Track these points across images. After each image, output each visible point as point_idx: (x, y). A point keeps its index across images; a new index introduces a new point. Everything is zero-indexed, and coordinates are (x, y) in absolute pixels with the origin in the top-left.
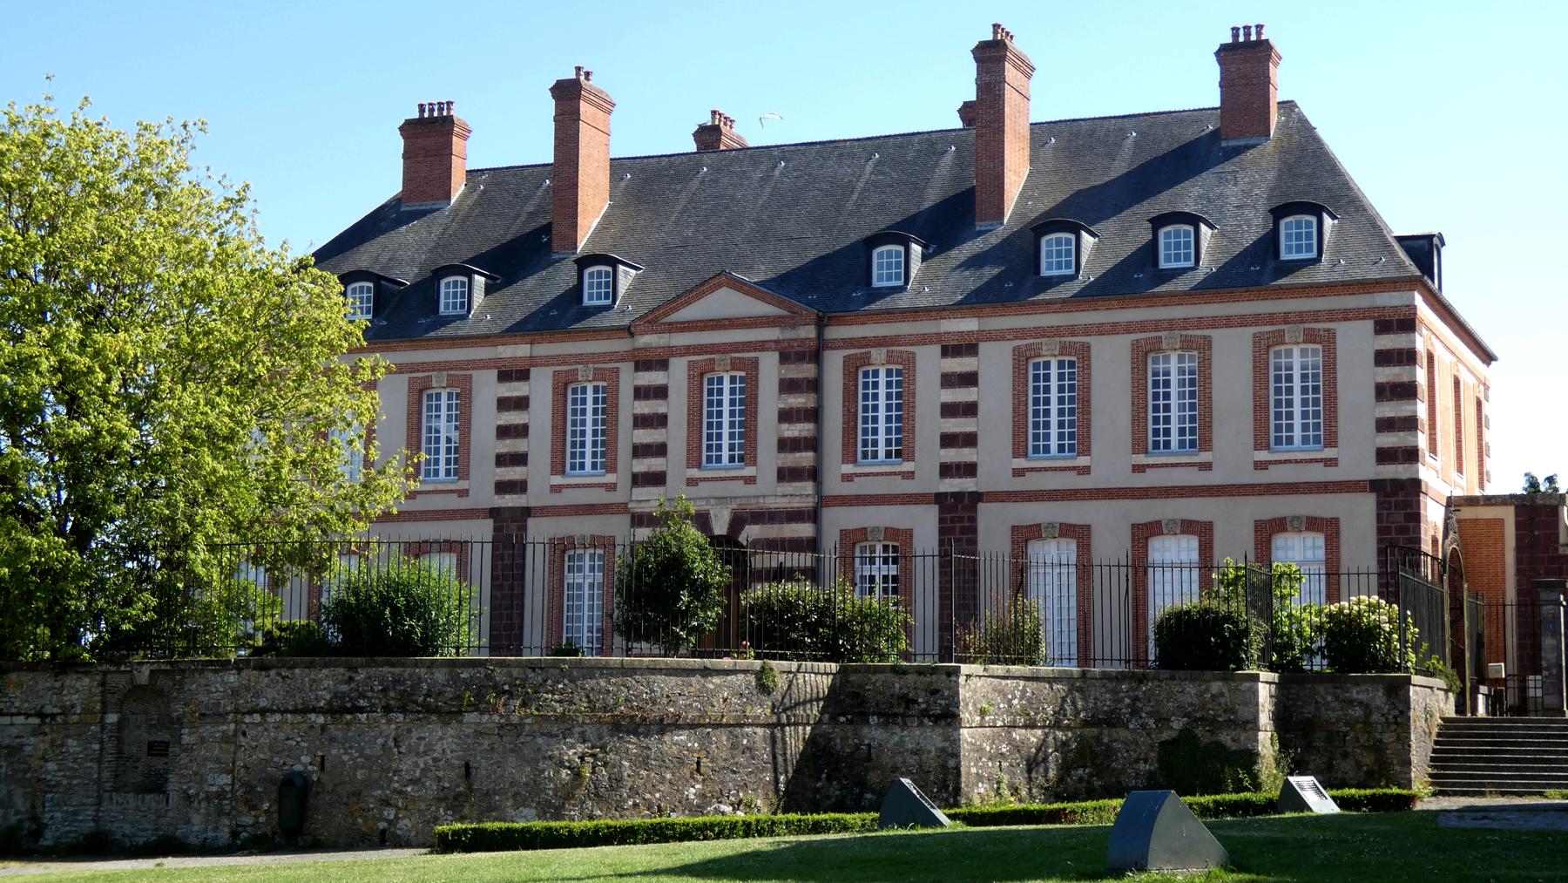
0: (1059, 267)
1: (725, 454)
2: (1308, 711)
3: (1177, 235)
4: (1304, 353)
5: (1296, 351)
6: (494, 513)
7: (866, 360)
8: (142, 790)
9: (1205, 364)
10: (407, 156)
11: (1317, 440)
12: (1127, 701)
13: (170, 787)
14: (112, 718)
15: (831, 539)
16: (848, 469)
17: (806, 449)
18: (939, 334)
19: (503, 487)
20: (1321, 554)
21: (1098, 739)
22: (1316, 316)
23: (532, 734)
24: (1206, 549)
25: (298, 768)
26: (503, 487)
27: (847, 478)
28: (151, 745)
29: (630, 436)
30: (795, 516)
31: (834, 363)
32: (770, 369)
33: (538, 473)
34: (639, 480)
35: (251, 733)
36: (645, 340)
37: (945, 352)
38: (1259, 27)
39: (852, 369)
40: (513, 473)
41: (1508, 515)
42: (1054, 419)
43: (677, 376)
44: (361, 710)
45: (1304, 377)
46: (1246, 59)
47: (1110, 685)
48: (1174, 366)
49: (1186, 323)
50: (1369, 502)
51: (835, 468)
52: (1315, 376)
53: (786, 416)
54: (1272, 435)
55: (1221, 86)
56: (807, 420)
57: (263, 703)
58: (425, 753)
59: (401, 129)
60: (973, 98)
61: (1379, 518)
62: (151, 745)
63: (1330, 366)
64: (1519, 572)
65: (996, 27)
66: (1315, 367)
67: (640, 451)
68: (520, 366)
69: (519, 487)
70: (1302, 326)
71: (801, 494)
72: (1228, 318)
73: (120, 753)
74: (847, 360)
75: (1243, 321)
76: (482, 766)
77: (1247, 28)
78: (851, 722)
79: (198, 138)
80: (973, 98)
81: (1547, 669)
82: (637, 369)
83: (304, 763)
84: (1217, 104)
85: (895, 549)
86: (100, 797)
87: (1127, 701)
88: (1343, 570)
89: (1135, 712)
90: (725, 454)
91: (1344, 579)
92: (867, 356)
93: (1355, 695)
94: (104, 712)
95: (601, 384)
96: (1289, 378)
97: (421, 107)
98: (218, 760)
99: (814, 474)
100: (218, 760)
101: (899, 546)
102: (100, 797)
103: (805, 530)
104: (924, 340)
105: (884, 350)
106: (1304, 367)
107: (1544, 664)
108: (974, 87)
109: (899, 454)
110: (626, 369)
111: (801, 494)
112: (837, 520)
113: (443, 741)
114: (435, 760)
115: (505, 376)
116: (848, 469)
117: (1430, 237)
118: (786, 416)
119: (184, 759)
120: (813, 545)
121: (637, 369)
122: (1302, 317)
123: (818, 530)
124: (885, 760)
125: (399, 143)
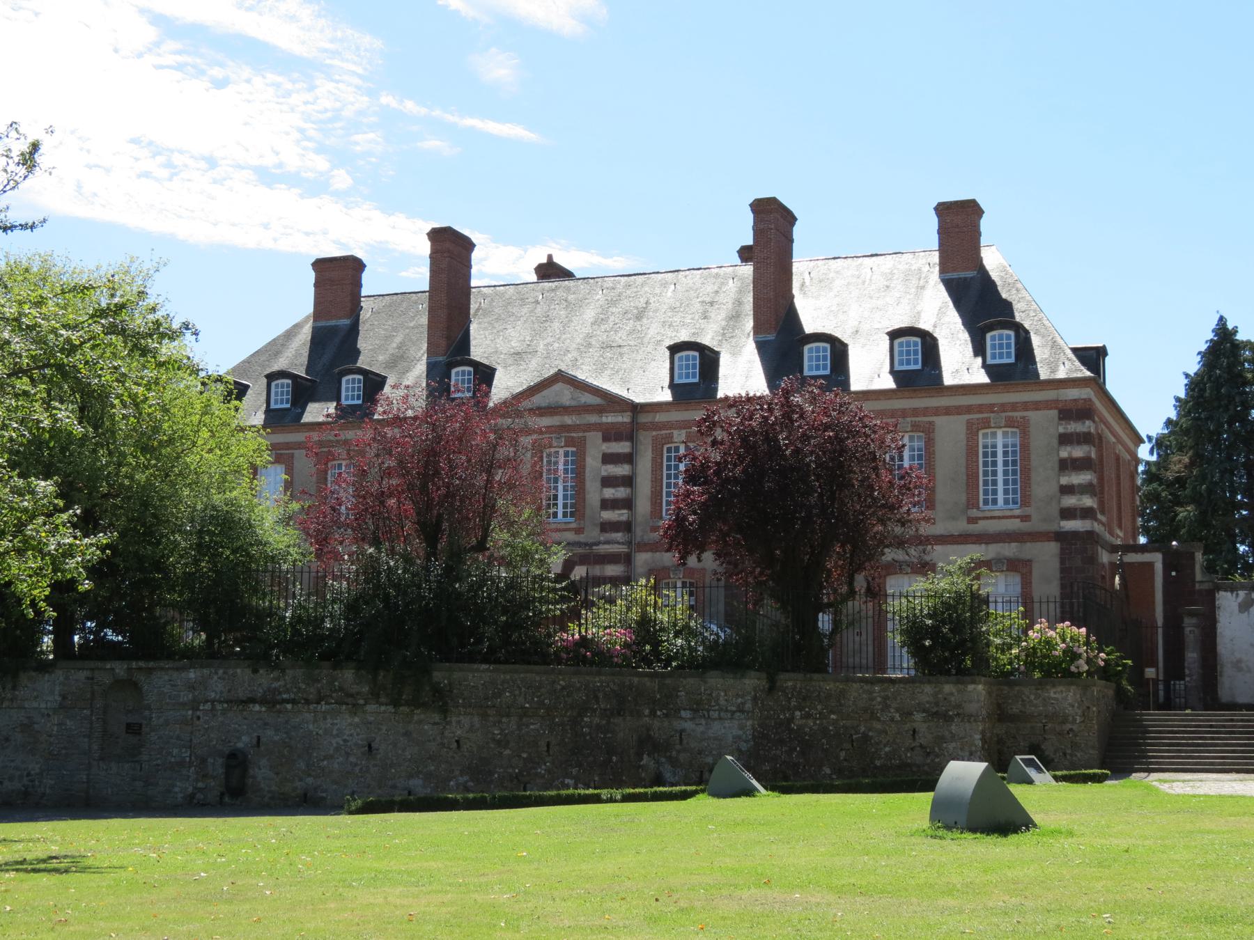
0: (908, 363)
3: (1001, 337)
4: (1005, 434)
5: (1000, 433)
7: (669, 439)
9: (930, 442)
10: (317, 285)
11: (1015, 503)
12: (879, 699)
17: (623, 508)
18: (1057, 401)
20: (1018, 589)
22: (1014, 407)
24: (1026, 584)
25: (240, 745)
28: (129, 726)
31: (646, 441)
32: (596, 447)
37: (606, 439)
42: (1000, 478)
45: (1005, 453)
47: (866, 687)
48: (1000, 442)
49: (916, 412)
50: (1053, 548)
52: (1014, 452)
54: (981, 497)
55: (939, 233)
56: (624, 485)
58: (337, 735)
59: (936, 209)
60: (750, 242)
62: (129, 726)
63: (1025, 447)
64: (1165, 603)
66: (1014, 445)
70: (1004, 415)
72: (937, 408)
74: (655, 439)
78: (666, 716)
79: (162, 270)
80: (750, 242)
81: (1190, 675)
83: (244, 742)
84: (427, 289)
85: (691, 584)
87: (879, 699)
88: (1036, 599)
91: (1036, 606)
92: (671, 436)
93: (1052, 695)
95: (570, 449)
96: (994, 454)
100: (178, 738)
105: (684, 431)
106: (1005, 446)
107: (1187, 672)
108: (751, 232)
110: (594, 438)
114: (345, 741)
117: (1097, 349)
118: (607, 482)
122: (1003, 407)
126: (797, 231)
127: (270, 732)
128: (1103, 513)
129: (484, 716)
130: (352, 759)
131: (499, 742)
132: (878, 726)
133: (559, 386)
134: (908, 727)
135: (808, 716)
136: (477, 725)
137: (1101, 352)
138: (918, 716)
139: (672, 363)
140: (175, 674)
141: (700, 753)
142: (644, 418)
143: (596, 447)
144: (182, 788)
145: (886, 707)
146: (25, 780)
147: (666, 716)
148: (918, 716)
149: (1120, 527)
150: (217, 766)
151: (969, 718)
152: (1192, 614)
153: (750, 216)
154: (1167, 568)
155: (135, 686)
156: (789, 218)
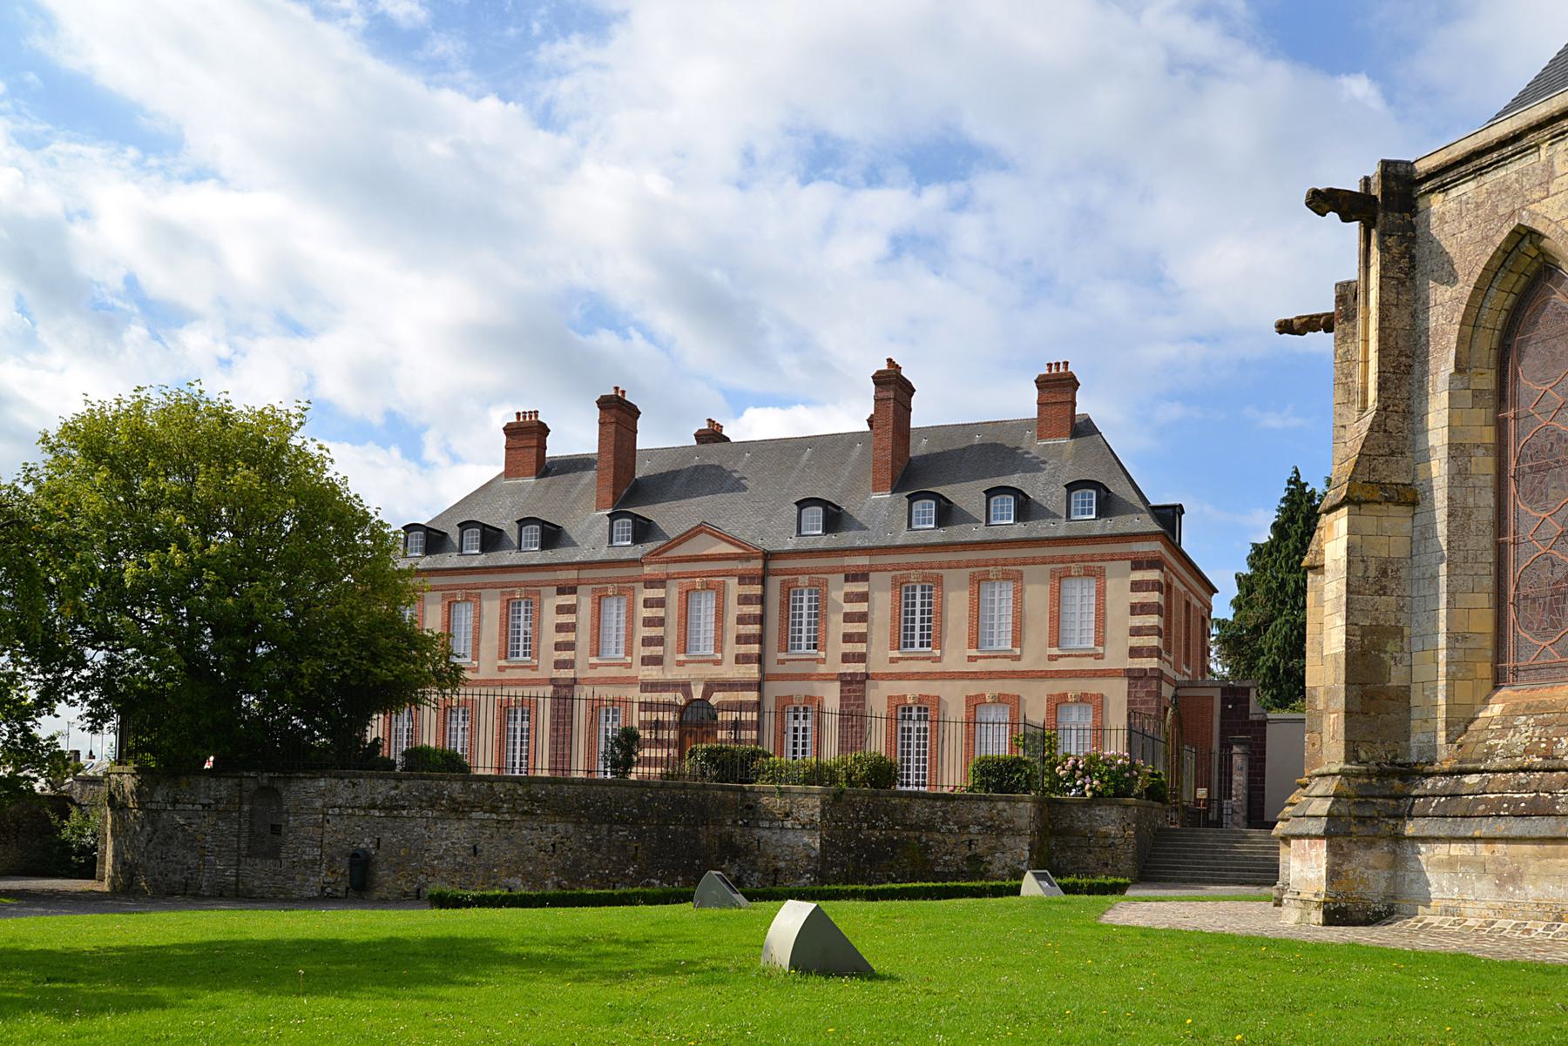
1: (804, 642)
2: (1065, 823)
6: (552, 681)
8: (266, 856)
13: (284, 855)
14: (246, 808)
15: (770, 705)
16: (782, 656)
19: (559, 665)
21: (918, 839)
23: (520, 828)
26: (559, 665)
27: (781, 662)
29: (643, 632)
30: (745, 686)
31: (774, 583)
33: (582, 656)
34: (646, 661)
35: (333, 822)
36: (647, 570)
38: (1066, 364)
39: (787, 590)
40: (566, 655)
41: (1217, 695)
43: (673, 593)
44: (404, 808)
46: (1057, 386)
49: (1005, 563)
50: (1122, 685)
51: (774, 655)
53: (741, 620)
57: (340, 801)
61: (1129, 693)
65: (890, 360)
67: (647, 642)
68: (572, 583)
69: (569, 664)
71: (752, 672)
73: (252, 831)
74: (783, 582)
75: (1044, 561)
76: (483, 845)
77: (1058, 364)
82: (847, 580)
83: (366, 843)
86: (239, 861)
89: (945, 821)
90: (804, 642)
94: (241, 804)
97: (1050, 365)
98: (311, 839)
99: (760, 659)
100: (311, 839)
101: (814, 706)
102: (239, 861)
103: (752, 696)
104: (833, 571)
109: (815, 647)
110: (733, 582)
111: (752, 672)
112: (775, 689)
113: (458, 832)
115: (561, 591)
116: (782, 656)
117: (1173, 507)
118: (741, 620)
119: (291, 837)
120: (758, 706)
121: (847, 580)
123: (761, 696)
124: (770, 851)
125: (502, 439)
126: (915, 401)
127: (388, 834)
128: (1169, 652)
129: (578, 823)
130: (459, 859)
131: (590, 846)
132: (938, 837)
133: (703, 538)
134: (965, 838)
135: (874, 827)
136: (571, 831)
137: (1178, 510)
138: (974, 829)
139: (611, 526)
140: (308, 783)
141: (775, 858)
142: (775, 565)
143: (734, 588)
144: (313, 884)
145: (945, 821)
146: (186, 874)
147: (746, 825)
148: (974, 829)
149: (1188, 666)
150: (343, 866)
151: (1018, 833)
152: (1239, 743)
153: (504, 437)
154: (1224, 701)
155: (277, 793)
156: (907, 389)
